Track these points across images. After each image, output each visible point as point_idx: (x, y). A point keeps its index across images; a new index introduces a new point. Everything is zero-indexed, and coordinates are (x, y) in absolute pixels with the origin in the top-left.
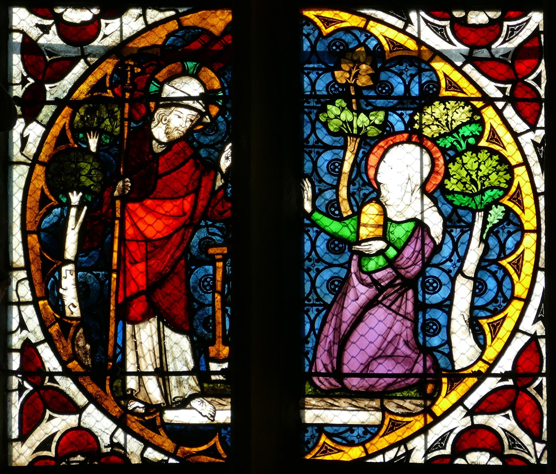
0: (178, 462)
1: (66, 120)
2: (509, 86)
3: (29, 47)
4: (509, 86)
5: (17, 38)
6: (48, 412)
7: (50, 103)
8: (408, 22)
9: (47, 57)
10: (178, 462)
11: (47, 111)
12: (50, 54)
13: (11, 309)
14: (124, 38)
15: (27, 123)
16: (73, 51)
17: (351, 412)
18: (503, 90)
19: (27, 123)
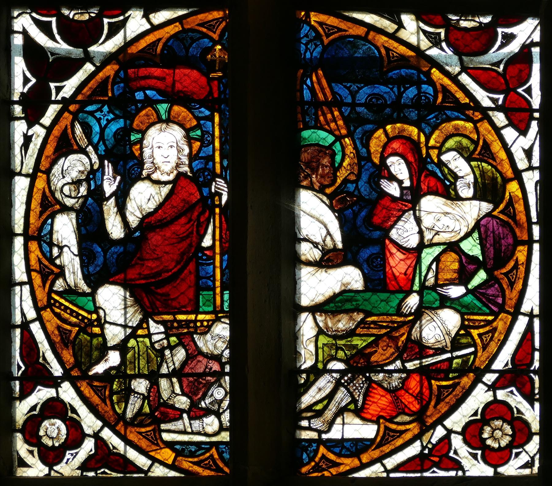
0: (183, 475)
1: (38, 253)
2: (501, 97)
3: (32, 50)
4: (501, 97)
5: (18, 40)
6: (52, 85)
7: (56, 102)
8: (401, 26)
9: (69, 412)
10: (183, 475)
11: (52, 110)
12: (52, 54)
13: (15, 403)
14: (128, 39)
15: (30, 126)
16: (77, 52)
17: (20, 154)
18: (494, 101)
19: (30, 126)
